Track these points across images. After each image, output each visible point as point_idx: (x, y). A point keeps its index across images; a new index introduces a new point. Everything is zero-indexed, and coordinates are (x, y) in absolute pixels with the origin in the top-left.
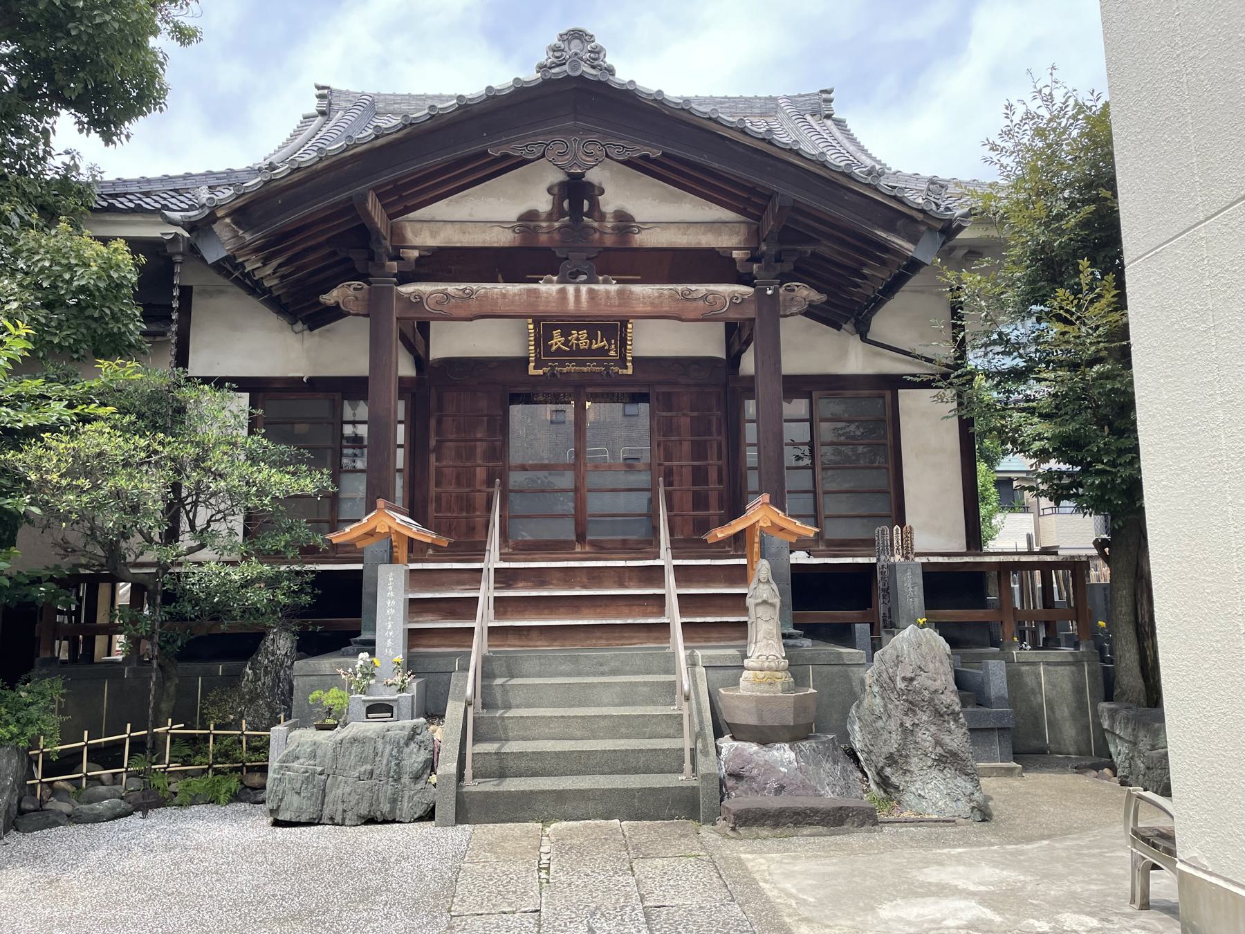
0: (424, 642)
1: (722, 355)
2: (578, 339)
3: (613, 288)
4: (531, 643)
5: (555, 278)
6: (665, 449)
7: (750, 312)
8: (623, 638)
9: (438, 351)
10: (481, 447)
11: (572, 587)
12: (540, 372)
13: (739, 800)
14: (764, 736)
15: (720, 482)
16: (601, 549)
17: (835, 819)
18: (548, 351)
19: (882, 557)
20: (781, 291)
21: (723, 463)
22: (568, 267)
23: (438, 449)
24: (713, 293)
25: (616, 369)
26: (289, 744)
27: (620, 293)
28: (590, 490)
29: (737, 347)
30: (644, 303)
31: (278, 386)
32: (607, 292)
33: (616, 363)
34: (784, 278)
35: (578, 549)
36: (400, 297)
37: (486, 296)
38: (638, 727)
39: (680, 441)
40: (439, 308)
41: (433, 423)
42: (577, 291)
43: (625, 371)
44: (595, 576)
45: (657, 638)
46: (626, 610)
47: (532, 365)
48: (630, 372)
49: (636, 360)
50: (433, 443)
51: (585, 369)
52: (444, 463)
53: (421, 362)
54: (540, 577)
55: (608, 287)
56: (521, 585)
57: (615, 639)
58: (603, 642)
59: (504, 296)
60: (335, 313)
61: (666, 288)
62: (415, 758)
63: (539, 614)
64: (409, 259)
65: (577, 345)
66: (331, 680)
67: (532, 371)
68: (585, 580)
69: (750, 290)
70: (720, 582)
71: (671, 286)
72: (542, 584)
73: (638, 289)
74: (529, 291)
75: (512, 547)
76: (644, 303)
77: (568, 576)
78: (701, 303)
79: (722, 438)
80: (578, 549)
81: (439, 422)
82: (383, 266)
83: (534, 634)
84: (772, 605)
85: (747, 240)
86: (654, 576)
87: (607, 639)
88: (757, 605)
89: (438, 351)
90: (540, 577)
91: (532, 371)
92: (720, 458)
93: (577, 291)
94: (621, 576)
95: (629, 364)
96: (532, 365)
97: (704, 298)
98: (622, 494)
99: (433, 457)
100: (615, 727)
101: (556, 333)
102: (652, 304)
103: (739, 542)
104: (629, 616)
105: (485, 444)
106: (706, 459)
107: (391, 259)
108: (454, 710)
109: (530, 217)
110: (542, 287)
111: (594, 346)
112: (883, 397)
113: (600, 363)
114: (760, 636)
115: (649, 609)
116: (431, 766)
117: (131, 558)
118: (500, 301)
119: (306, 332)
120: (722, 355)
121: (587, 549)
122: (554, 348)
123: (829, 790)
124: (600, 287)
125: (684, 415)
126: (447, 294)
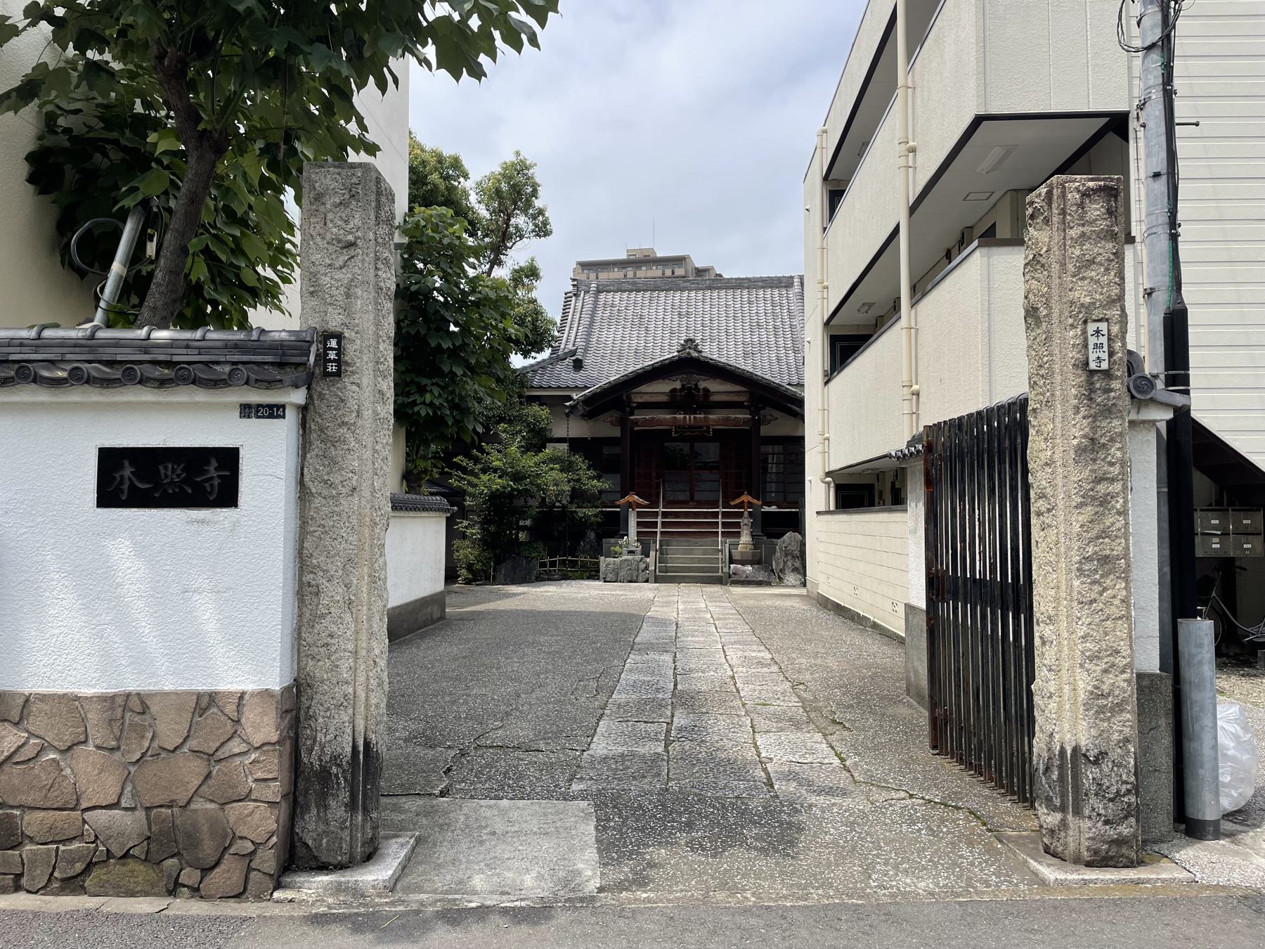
13: (736, 578)
14: (743, 563)
16: (700, 505)
17: (759, 584)
26: (604, 562)
38: (708, 561)
60: (521, 322)
62: (642, 566)
66: (616, 544)
86: (655, 525)
90: (677, 515)
94: (705, 515)
100: (700, 561)
103: (741, 505)
108: (652, 554)
109: (674, 390)
116: (647, 568)
117: (282, 483)
123: (761, 576)
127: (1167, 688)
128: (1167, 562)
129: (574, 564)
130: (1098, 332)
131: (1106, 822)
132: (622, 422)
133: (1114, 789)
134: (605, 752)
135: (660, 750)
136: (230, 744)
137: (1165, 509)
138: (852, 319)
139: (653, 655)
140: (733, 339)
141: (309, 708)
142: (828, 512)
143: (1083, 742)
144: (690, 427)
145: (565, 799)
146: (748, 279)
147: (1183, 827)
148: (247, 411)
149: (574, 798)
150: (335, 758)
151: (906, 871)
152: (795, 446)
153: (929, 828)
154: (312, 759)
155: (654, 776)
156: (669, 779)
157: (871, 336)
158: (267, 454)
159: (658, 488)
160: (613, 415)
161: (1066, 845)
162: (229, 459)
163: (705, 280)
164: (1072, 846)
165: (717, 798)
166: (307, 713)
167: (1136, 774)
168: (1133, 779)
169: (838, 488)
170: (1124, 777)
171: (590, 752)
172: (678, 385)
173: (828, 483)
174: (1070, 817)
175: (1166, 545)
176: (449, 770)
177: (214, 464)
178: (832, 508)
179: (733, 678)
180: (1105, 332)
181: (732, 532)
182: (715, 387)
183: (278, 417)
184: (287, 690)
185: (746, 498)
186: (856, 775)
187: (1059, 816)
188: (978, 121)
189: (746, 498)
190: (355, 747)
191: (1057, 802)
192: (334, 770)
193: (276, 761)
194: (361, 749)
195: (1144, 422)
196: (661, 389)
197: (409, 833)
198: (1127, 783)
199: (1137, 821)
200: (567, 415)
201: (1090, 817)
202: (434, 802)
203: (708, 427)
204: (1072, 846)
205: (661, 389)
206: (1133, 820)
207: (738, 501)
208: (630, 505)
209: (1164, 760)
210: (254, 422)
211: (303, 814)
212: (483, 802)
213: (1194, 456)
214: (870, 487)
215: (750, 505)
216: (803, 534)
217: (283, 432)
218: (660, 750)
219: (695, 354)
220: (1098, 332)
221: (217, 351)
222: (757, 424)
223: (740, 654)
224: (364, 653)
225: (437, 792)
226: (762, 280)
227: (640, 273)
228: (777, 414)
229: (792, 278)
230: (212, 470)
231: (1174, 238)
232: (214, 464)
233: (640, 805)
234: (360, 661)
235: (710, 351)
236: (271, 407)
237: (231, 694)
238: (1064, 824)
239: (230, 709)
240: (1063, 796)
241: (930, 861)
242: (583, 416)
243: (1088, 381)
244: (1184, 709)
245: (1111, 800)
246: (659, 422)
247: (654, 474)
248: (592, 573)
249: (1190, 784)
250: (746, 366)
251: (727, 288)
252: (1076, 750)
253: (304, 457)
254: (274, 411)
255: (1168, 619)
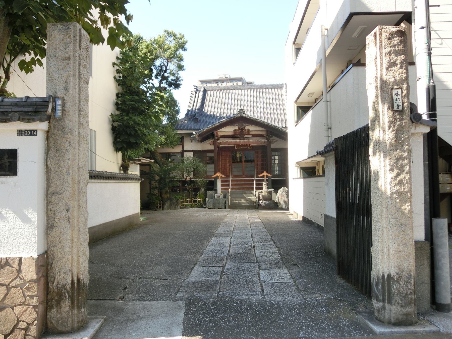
86: (228, 185)
109: (235, 130)
127: (427, 247)
128: (428, 194)
129: (195, 201)
130: (397, 93)
131: (401, 306)
132: (214, 144)
133: (405, 292)
134: (194, 280)
135: (218, 278)
136: (15, 281)
137: (427, 171)
138: (305, 100)
139: (222, 238)
140: (258, 109)
141: (52, 264)
142: (297, 178)
143: (393, 273)
144: (242, 145)
145: (173, 301)
146: (266, 85)
147: (434, 307)
148: (20, 133)
149: (177, 300)
150: (64, 286)
151: (316, 329)
152: (283, 153)
153: (328, 310)
154: (53, 287)
155: (213, 290)
156: (220, 291)
157: (312, 106)
158: (31, 152)
159: (230, 170)
160: (209, 141)
161: (384, 316)
162: (12, 154)
163: (249, 85)
164: (387, 316)
165: (238, 300)
166: (51, 266)
167: (414, 285)
168: (413, 288)
169: (302, 168)
170: (409, 287)
171: (188, 280)
172: (237, 128)
173: (298, 167)
174: (386, 305)
175: (428, 186)
176: (126, 288)
177: (6, 157)
178: (299, 177)
179: (254, 246)
180: (400, 93)
181: (260, 188)
182: (253, 129)
183: (34, 135)
184: (40, 256)
185: (265, 173)
186: (299, 287)
187: (381, 304)
188: (352, 15)
189: (265, 173)
190: (73, 281)
191: (381, 298)
192: (64, 291)
193: (36, 287)
194: (76, 281)
195: (417, 133)
196: (229, 130)
197: (101, 317)
198: (410, 289)
199: (415, 305)
200: (192, 141)
201: (394, 304)
202: (116, 302)
203: (250, 145)
204: (387, 316)
205: (229, 130)
206: (413, 305)
207: (262, 175)
208: (217, 177)
209: (427, 278)
210: (23, 137)
211: (50, 310)
212: (137, 303)
213: (433, 141)
214: (314, 168)
215: (267, 176)
216: (288, 187)
217: (38, 142)
218: (218, 278)
219: (244, 115)
220: (397, 93)
221: (8, 107)
222: (269, 143)
223: (258, 237)
224: (75, 240)
225: (117, 298)
226: (271, 85)
227: (224, 84)
228: (277, 139)
229: (283, 84)
230: (6, 160)
231: (430, 55)
232: (6, 157)
233: (205, 303)
234: (74, 244)
235: (251, 114)
236: (31, 131)
237: (14, 259)
238: (384, 307)
239: (16, 265)
240: (384, 295)
241: (327, 324)
242: (199, 141)
243: (393, 115)
244: (435, 256)
245: (403, 297)
246: (230, 143)
247: (228, 164)
248: (203, 205)
249: (438, 288)
250: (265, 120)
251: (257, 89)
252: (389, 275)
253: (48, 153)
254: (32, 133)
255: (428, 218)
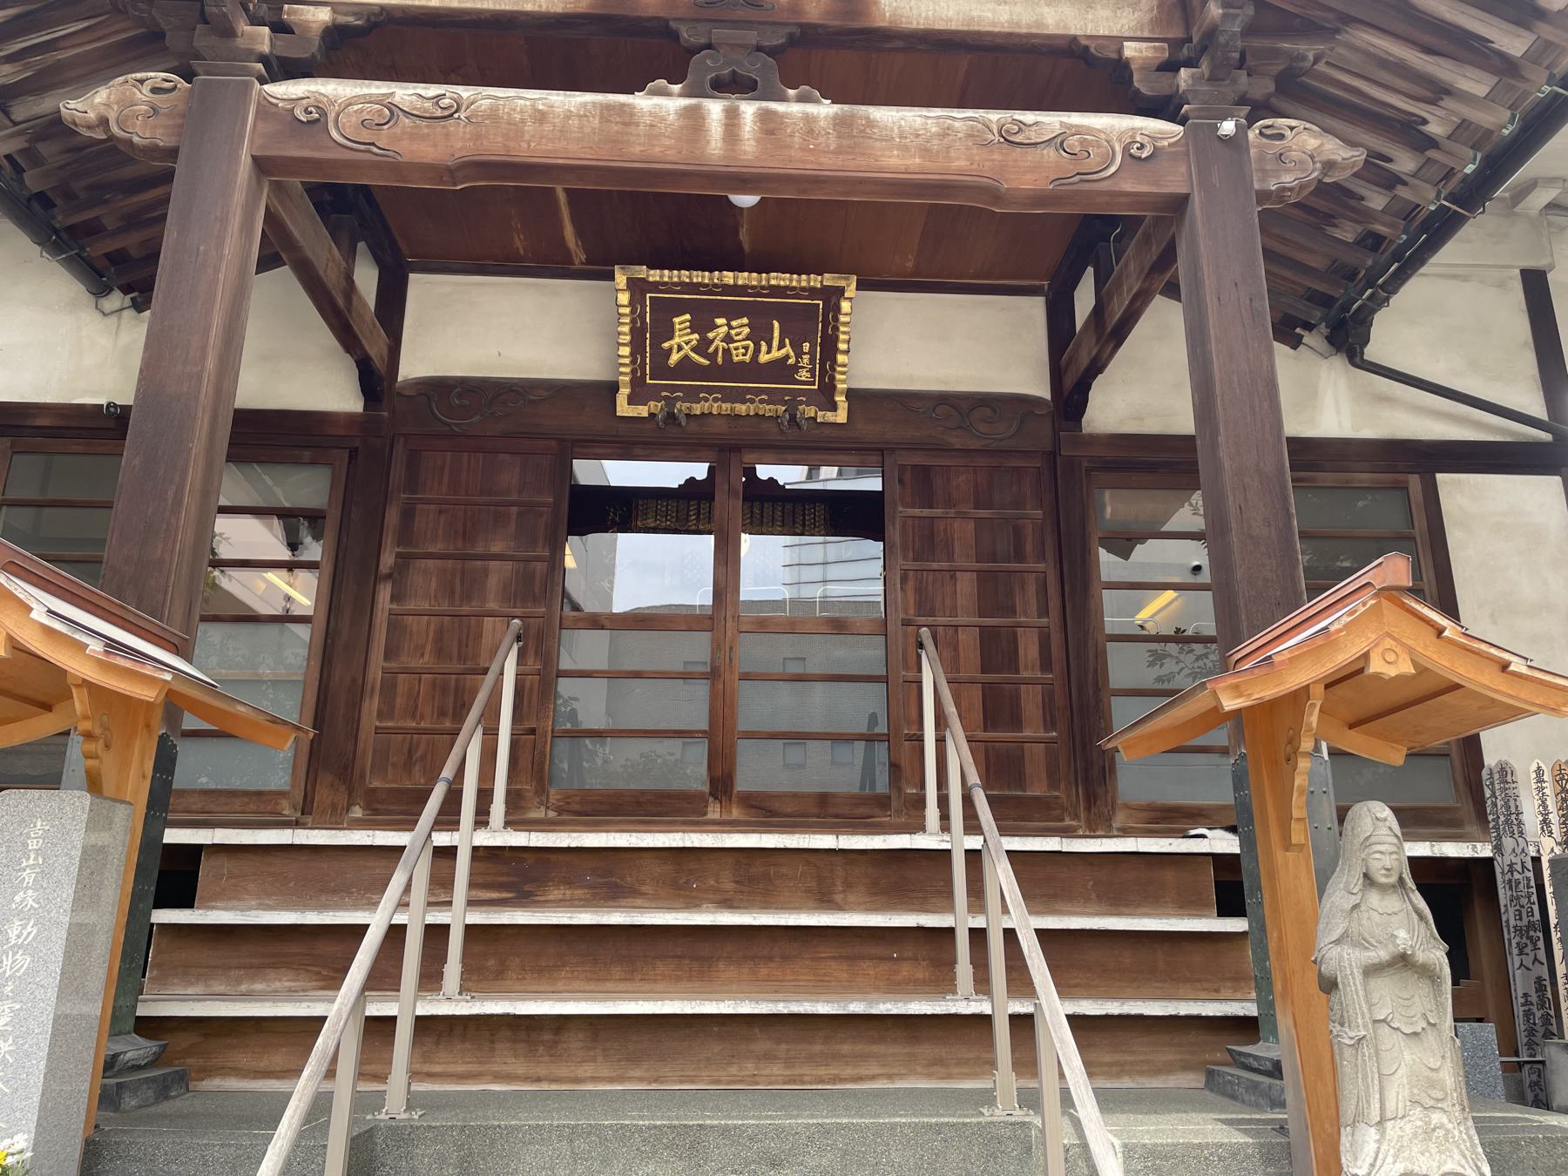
0: (243, 1059)
1: (1037, 386)
2: (728, 339)
3: (825, 110)
4: (563, 1071)
5: (676, 88)
6: (919, 590)
7: (1174, 182)
8: (837, 1057)
9: (420, 360)
10: (498, 574)
11: (692, 904)
12: (643, 411)
15: (1046, 664)
18: (661, 370)
19: (1508, 843)
20: (1252, 135)
21: (1052, 621)
22: (708, 65)
23: (398, 576)
24: (1079, 130)
25: (810, 411)
27: (840, 122)
28: (746, 677)
29: (1069, 381)
30: (904, 149)
31: (39, 422)
32: (809, 119)
33: (811, 398)
34: (1259, 110)
35: (714, 812)
36: (267, 109)
37: (493, 115)
39: (953, 572)
40: (366, 136)
41: (392, 517)
42: (732, 116)
43: (830, 417)
44: (754, 874)
45: (939, 1062)
46: (839, 970)
47: (624, 392)
48: (841, 416)
49: (851, 394)
50: (388, 560)
51: (742, 409)
52: (410, 606)
53: (375, 379)
54: (609, 874)
55: (810, 108)
56: (555, 894)
57: (811, 1059)
58: (776, 1069)
59: (541, 117)
61: (961, 118)
63: (597, 981)
64: (305, 26)
65: (727, 352)
67: (623, 408)
68: (729, 886)
69: (1178, 129)
70: (1087, 900)
71: (970, 113)
72: (613, 894)
73: (885, 116)
74: (608, 107)
75: (534, 783)
76: (904, 149)
77: (683, 872)
78: (1050, 154)
79: (1047, 567)
80: (714, 812)
81: (408, 515)
82: (230, 33)
83: (574, 1041)
84: (1427, 973)
85: (1155, 22)
87: (789, 1062)
88: (1371, 971)
89: (420, 360)
90: (609, 874)
91: (623, 408)
92: (1044, 611)
93: (732, 116)
94: (824, 876)
95: (840, 399)
96: (624, 392)
97: (1058, 142)
98: (819, 687)
99: (384, 593)
101: (681, 321)
102: (925, 151)
104: (849, 989)
105: (509, 565)
106: (1012, 611)
107: (256, 21)
110: (641, 102)
111: (764, 358)
112: (1405, 488)
113: (774, 396)
114: (1397, 1095)
115: (906, 970)
118: (529, 128)
119: (129, 314)
120: (1037, 386)
121: (736, 813)
122: (675, 358)
124: (791, 109)
125: (964, 517)
126: (392, 107)
